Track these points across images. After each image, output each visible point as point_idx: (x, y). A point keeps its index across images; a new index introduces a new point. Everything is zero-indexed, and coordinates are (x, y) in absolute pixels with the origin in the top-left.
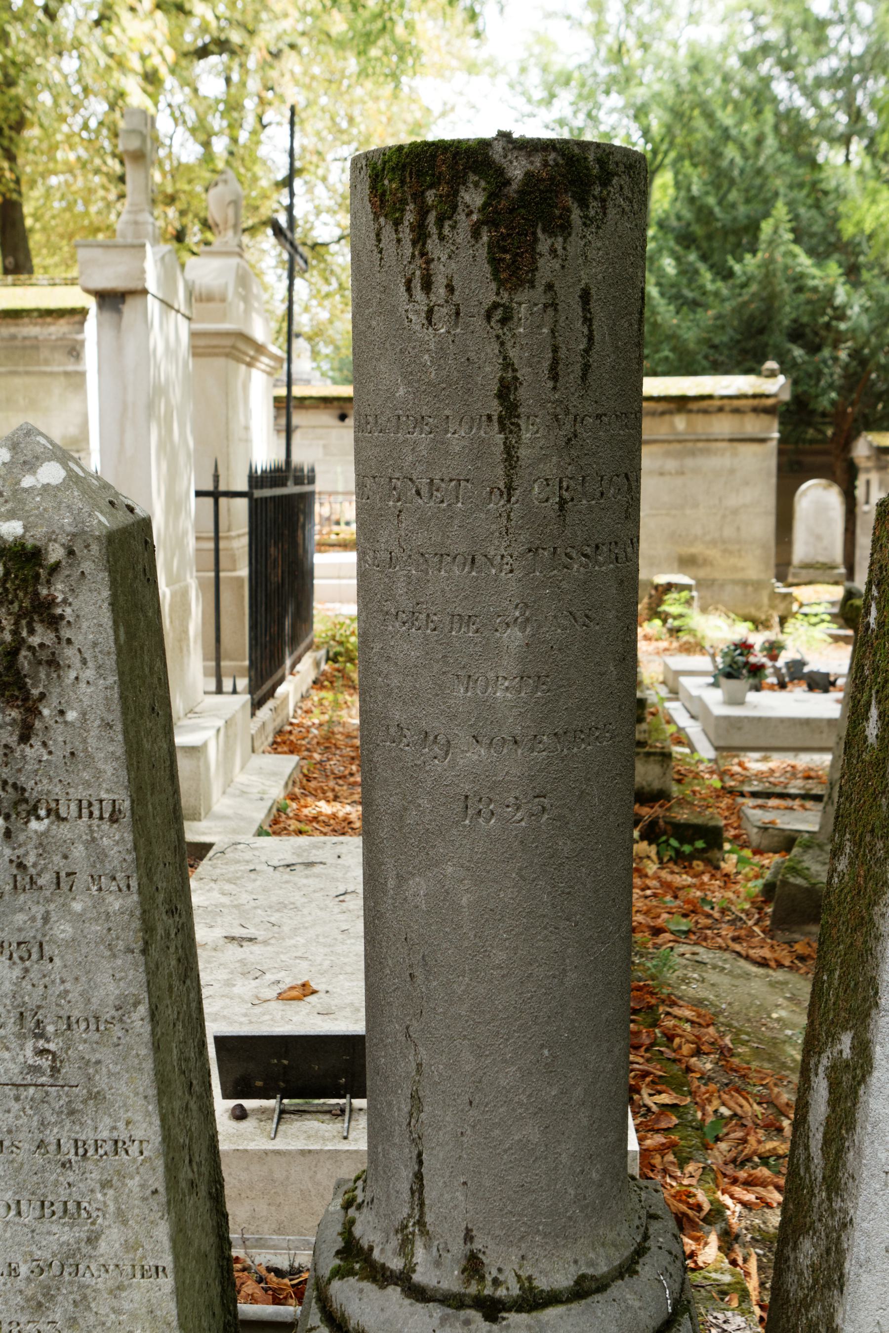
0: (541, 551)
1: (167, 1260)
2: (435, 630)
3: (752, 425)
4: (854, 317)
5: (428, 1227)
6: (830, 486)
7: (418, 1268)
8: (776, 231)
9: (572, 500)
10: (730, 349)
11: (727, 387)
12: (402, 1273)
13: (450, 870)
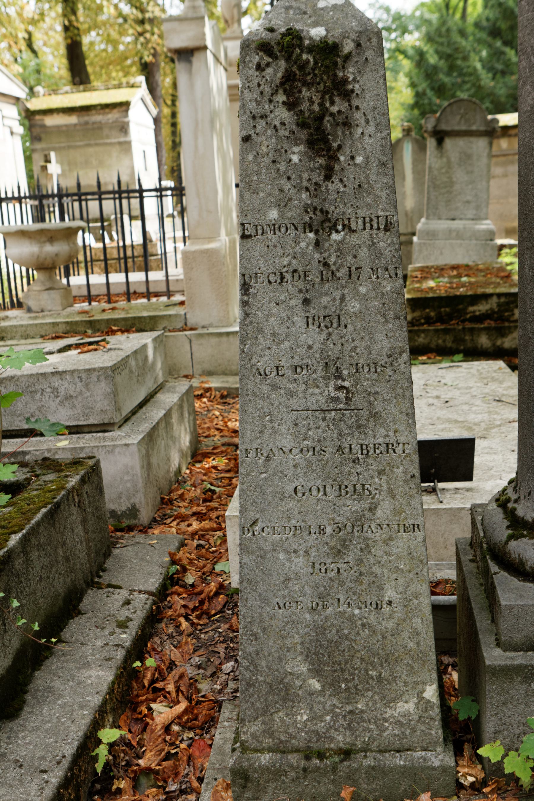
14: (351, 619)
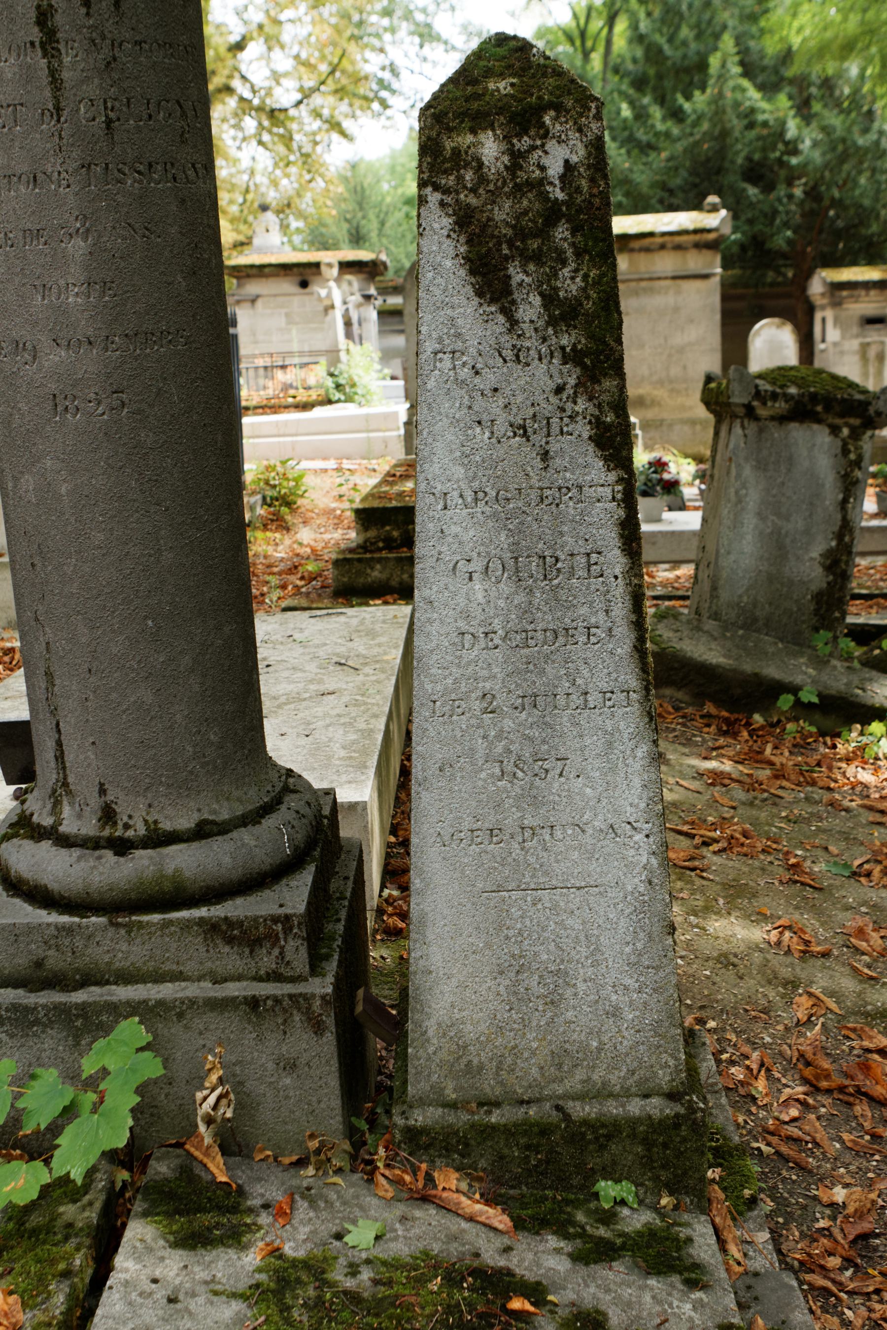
0: (93, 166)
2: (12, 246)
3: (695, 261)
4: (806, 151)
5: (71, 787)
6: (783, 324)
7: (64, 822)
8: (723, 65)
9: (119, 119)
10: (684, 191)
11: (668, 224)
12: (52, 828)
13: (49, 463)
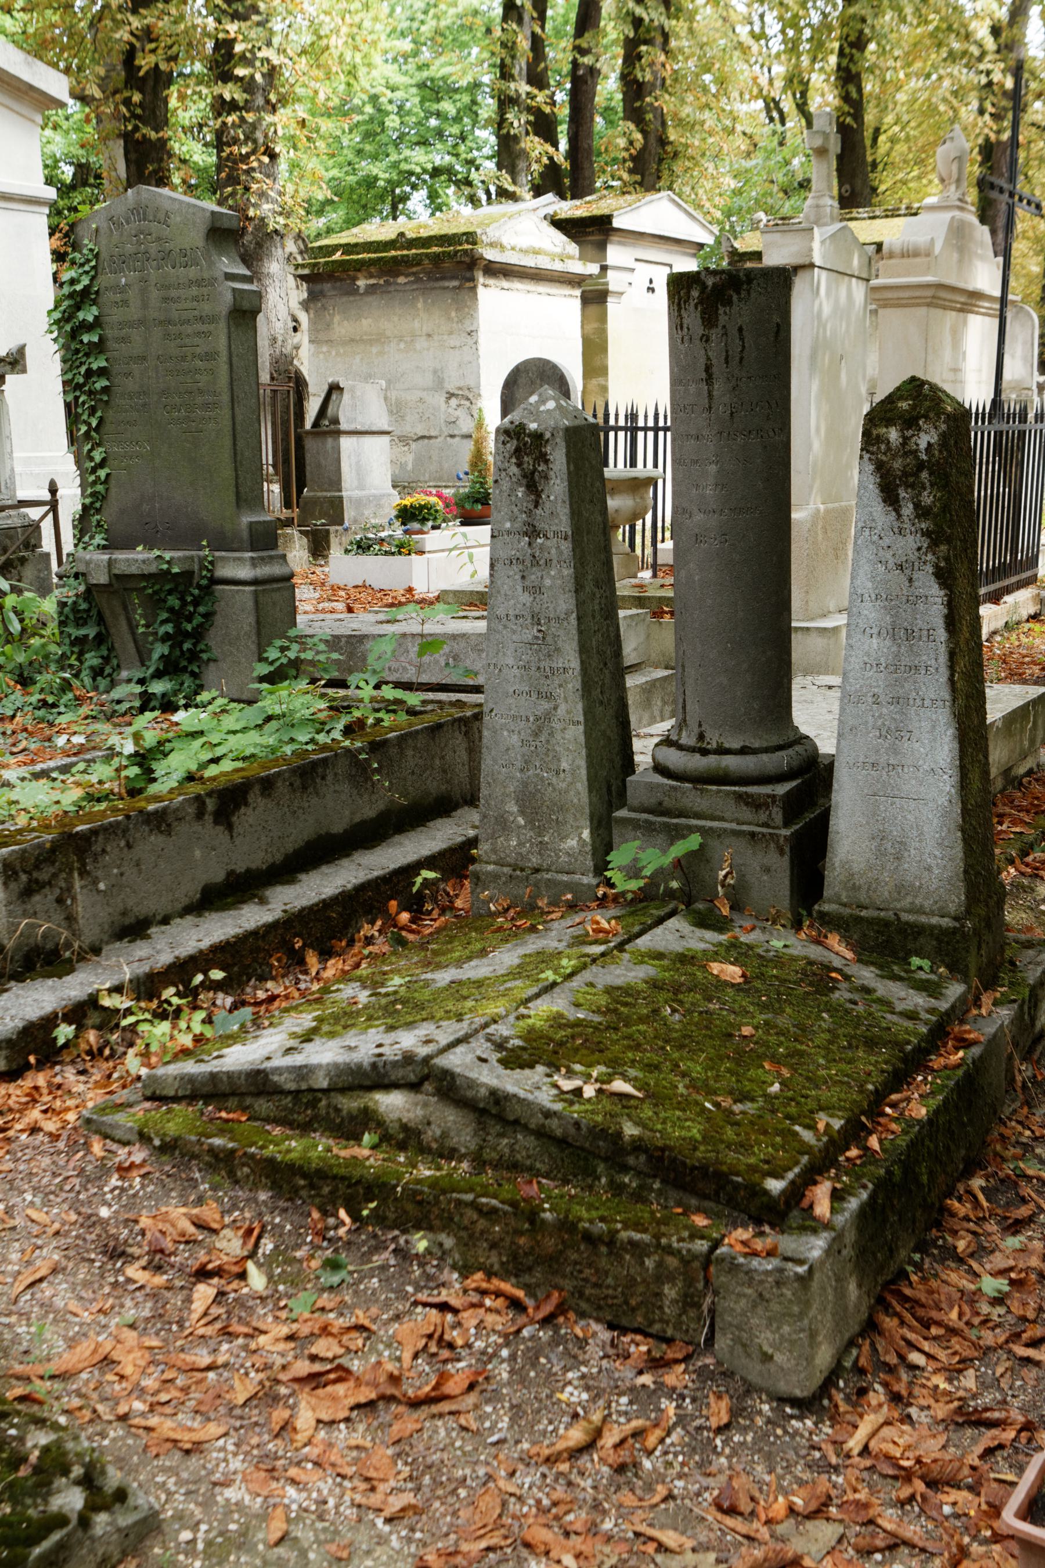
1: (581, 719)
14: (542, 779)
